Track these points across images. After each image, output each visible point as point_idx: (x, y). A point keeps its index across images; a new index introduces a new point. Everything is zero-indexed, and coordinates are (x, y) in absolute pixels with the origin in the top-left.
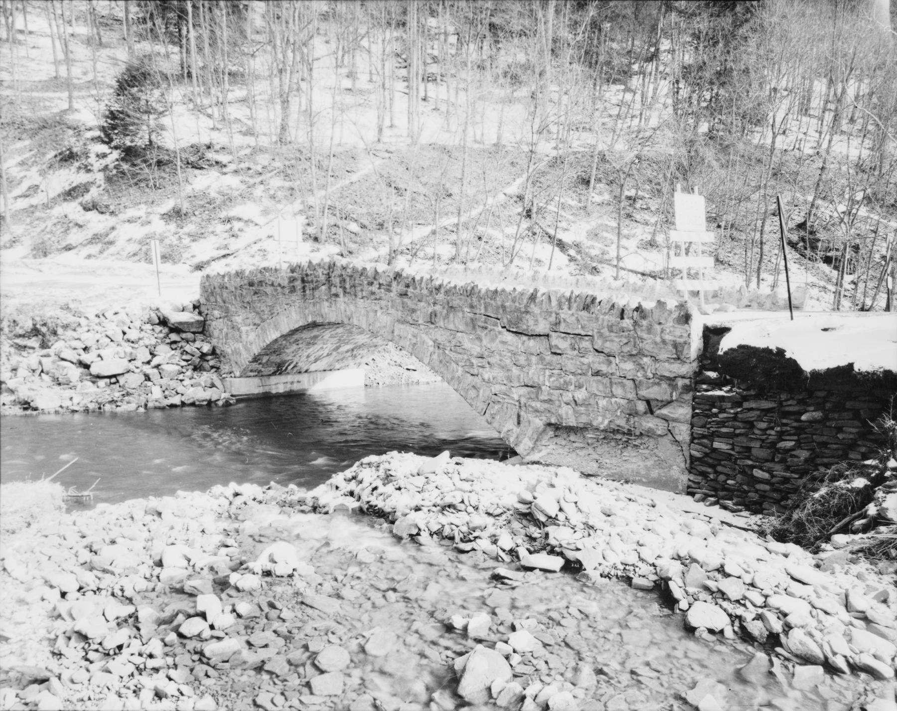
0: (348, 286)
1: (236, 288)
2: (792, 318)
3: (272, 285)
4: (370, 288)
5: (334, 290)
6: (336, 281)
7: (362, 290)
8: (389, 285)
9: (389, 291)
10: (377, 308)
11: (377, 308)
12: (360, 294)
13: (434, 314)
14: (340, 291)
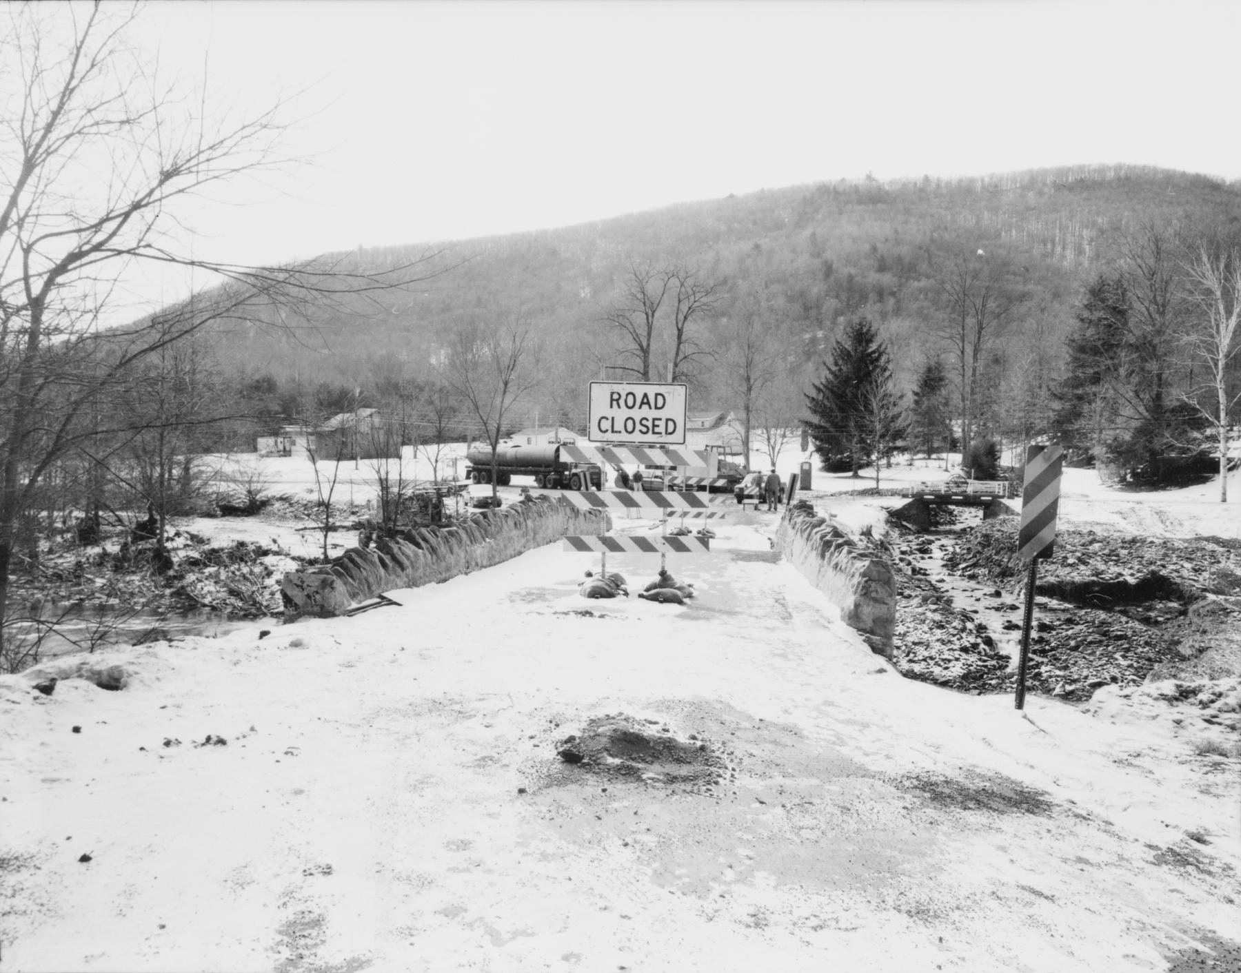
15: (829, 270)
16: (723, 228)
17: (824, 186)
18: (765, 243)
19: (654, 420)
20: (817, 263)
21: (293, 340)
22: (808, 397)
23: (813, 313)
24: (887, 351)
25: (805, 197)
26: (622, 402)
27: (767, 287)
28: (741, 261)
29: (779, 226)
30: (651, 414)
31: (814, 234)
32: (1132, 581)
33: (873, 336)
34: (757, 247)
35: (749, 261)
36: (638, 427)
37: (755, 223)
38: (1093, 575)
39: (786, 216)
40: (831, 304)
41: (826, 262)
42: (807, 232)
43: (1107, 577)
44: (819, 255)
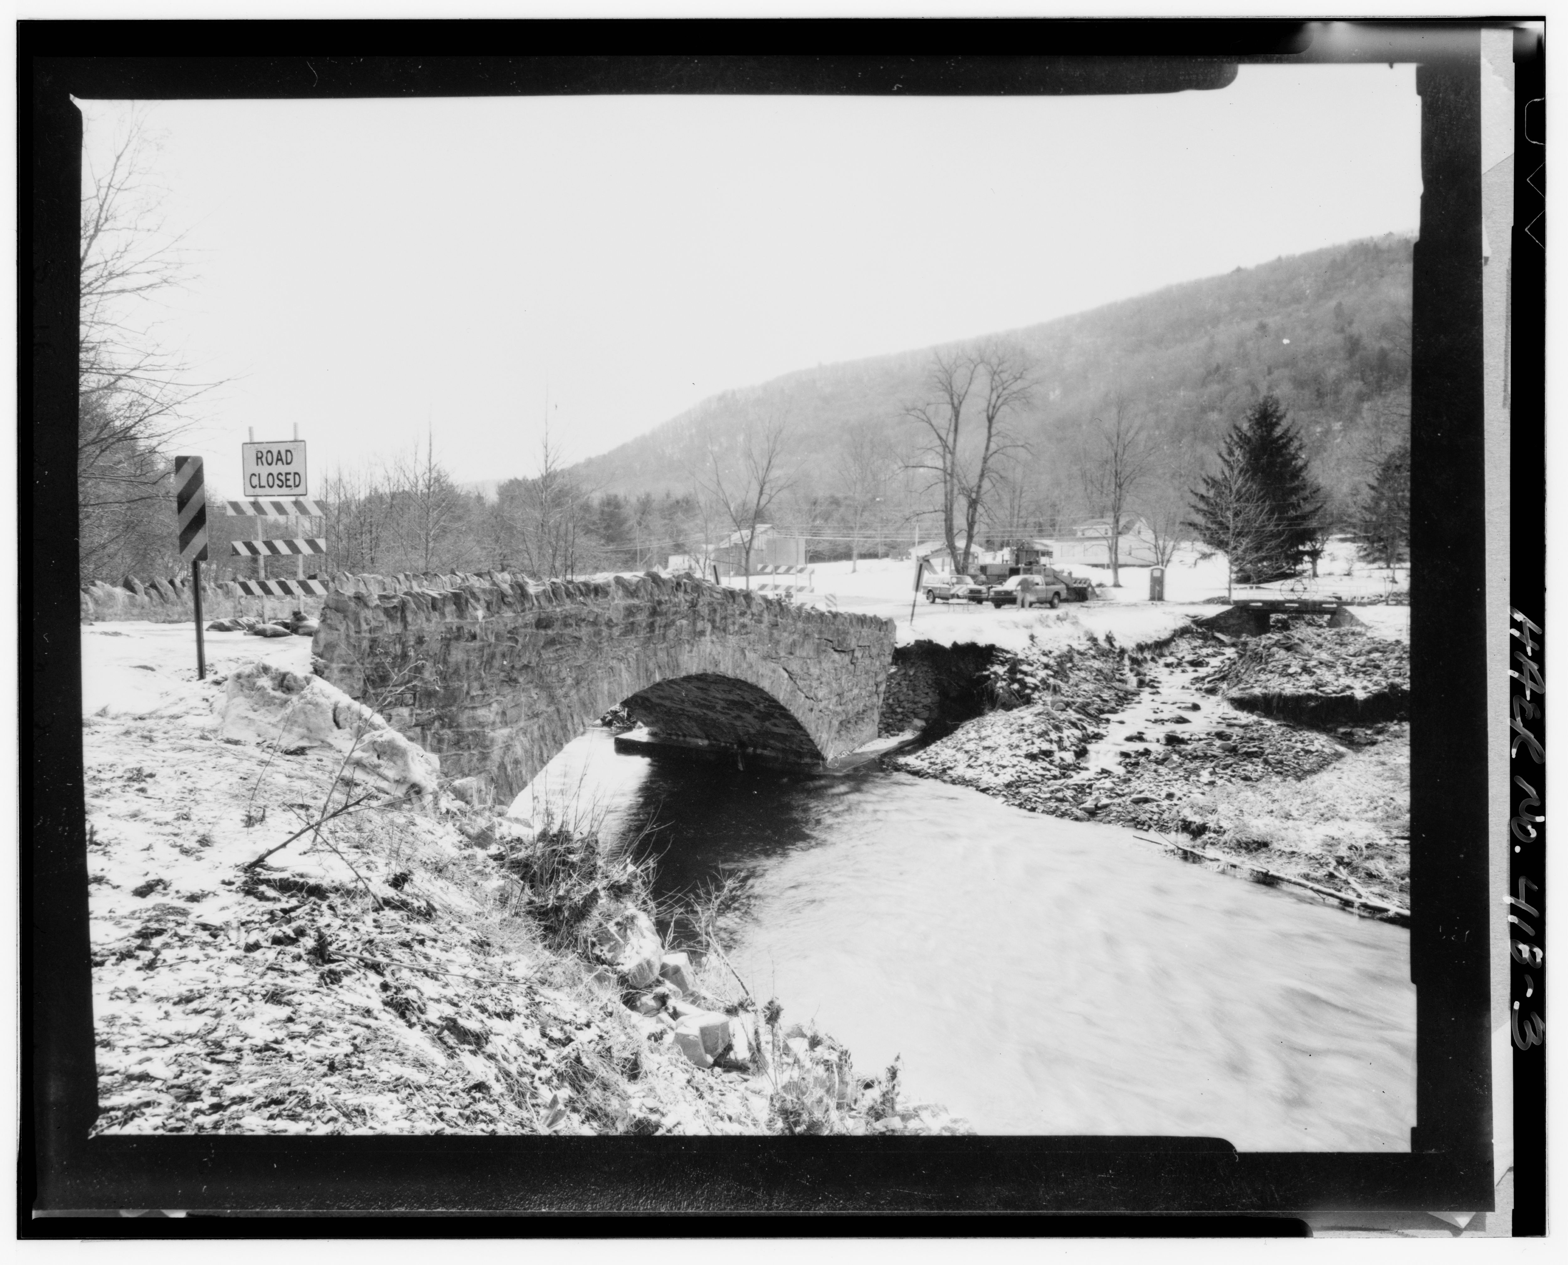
0: (718, 619)
1: (498, 636)
2: (295, 426)
3: (594, 623)
4: (742, 620)
5: (700, 625)
6: (705, 611)
7: (734, 623)
8: (761, 615)
9: (760, 622)
10: (745, 644)
11: (745, 644)
12: (731, 628)
13: (794, 644)
14: (709, 627)
15: (1353, 346)
16: (1226, 308)
17: (1362, 244)
18: (1273, 322)
19: (287, 474)
20: (1339, 338)
21: (1119, 469)
22: (1196, 494)
23: (1329, 400)
24: (1299, 436)
25: (1334, 261)
26: (264, 459)
27: (1270, 373)
28: (1241, 344)
29: (1297, 298)
30: (283, 468)
31: (1340, 304)
32: (1360, 695)
33: (1280, 418)
34: (1263, 327)
35: (1250, 344)
36: (277, 482)
37: (1265, 298)
38: (1312, 687)
39: (1308, 287)
40: (1355, 386)
41: (1351, 337)
42: (1333, 303)
43: (1328, 690)
44: (1342, 330)
